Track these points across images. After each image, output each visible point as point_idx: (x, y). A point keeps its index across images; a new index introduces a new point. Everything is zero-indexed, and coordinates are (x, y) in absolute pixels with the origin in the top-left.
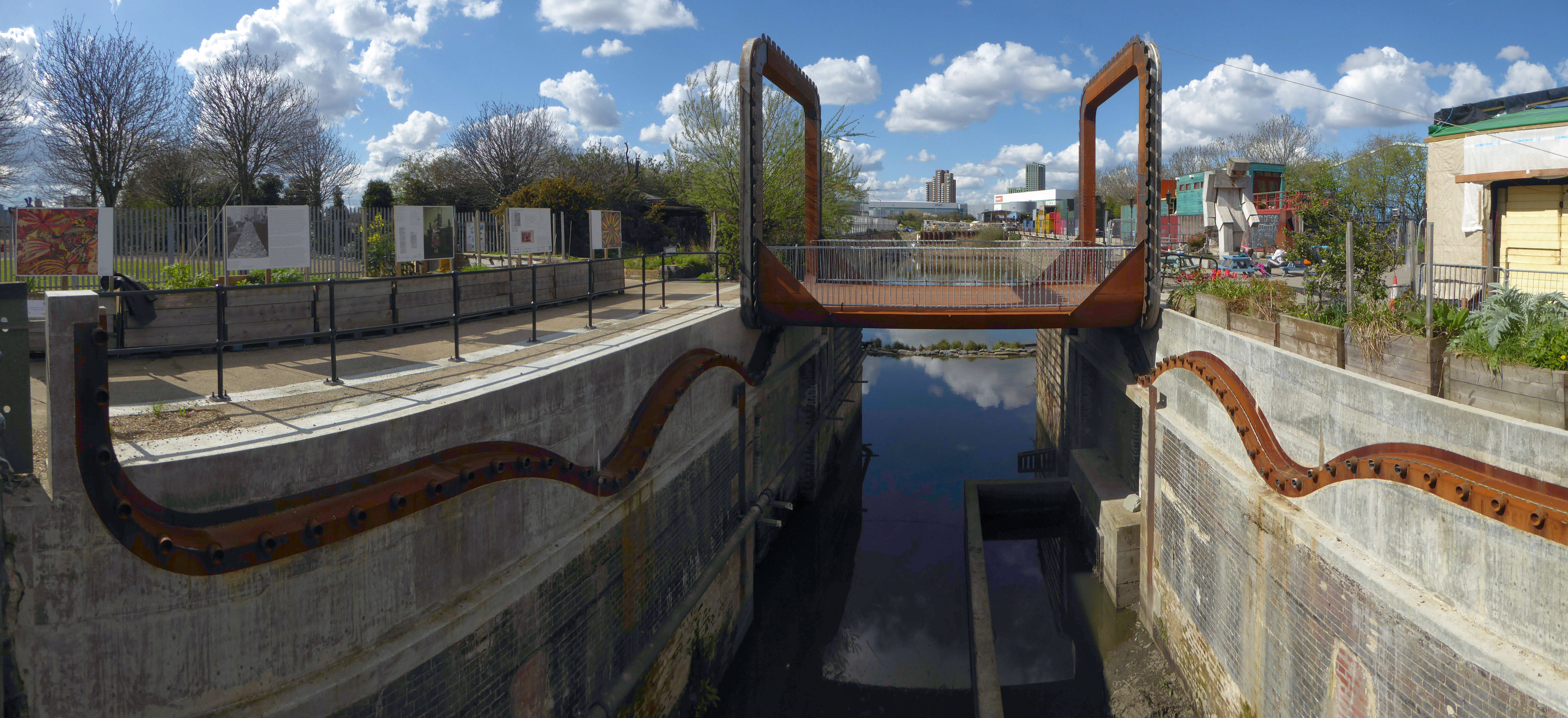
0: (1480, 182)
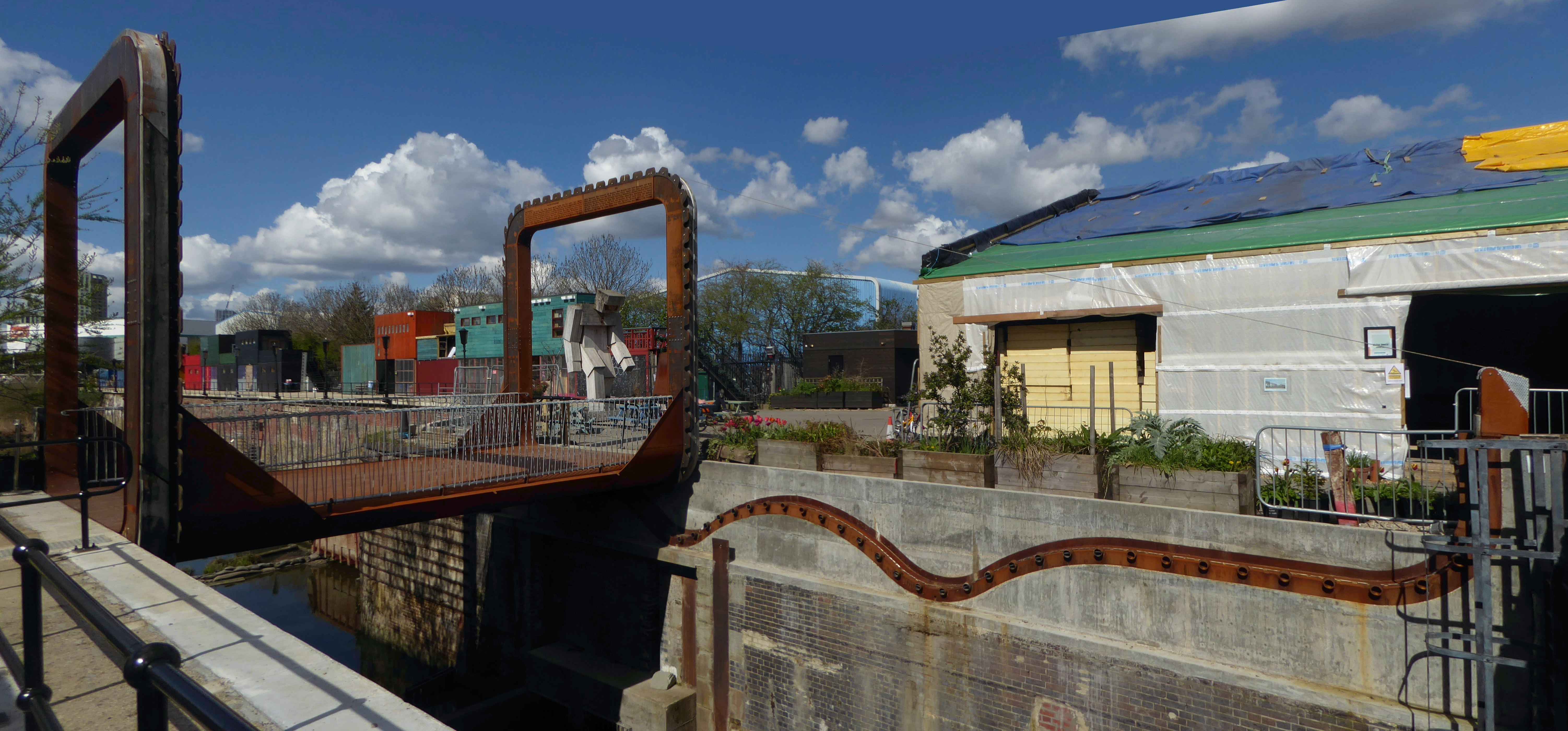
0: (984, 323)
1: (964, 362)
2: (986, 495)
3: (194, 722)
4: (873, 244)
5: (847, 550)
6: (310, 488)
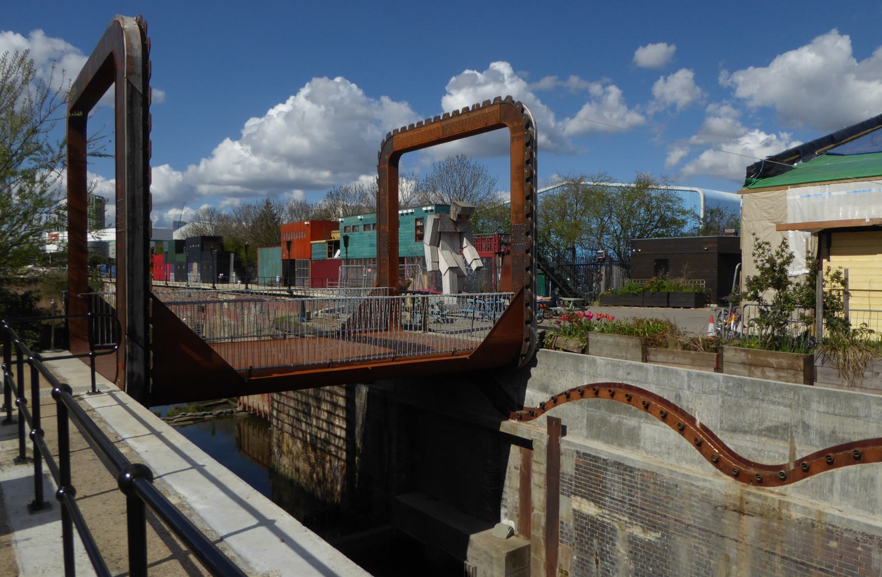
0: (808, 230)
1: (786, 267)
2: (805, 392)
3: (162, 523)
4: (698, 158)
5: (668, 433)
6: (236, 358)
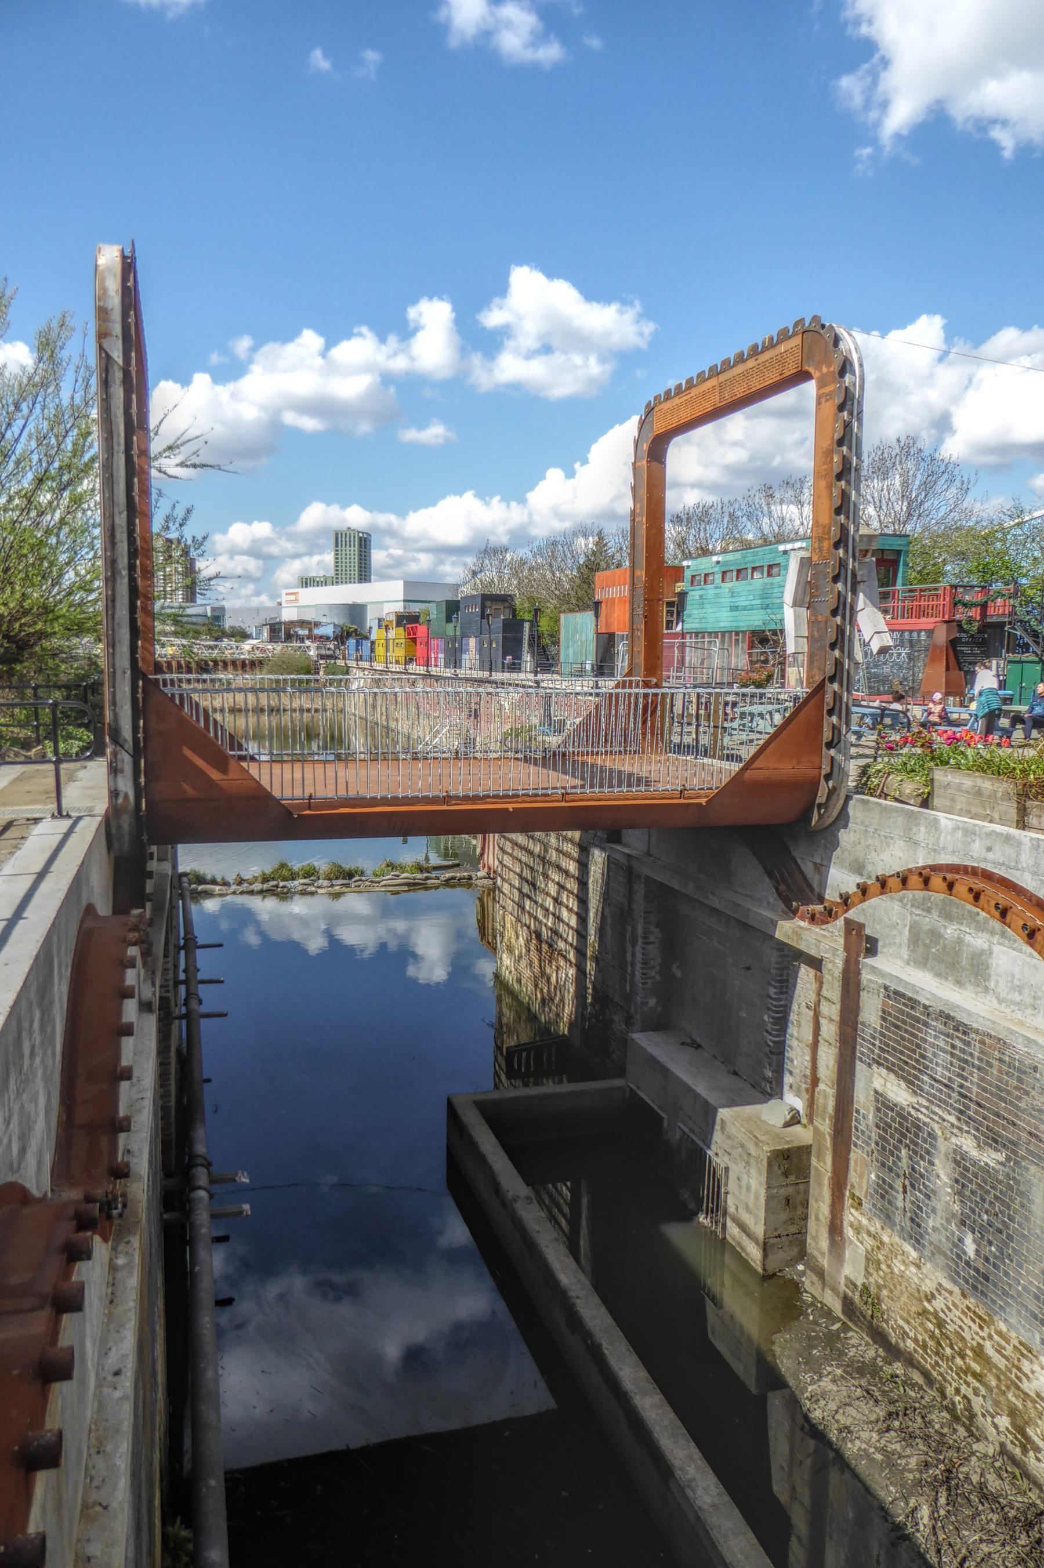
5: (1036, 967)
